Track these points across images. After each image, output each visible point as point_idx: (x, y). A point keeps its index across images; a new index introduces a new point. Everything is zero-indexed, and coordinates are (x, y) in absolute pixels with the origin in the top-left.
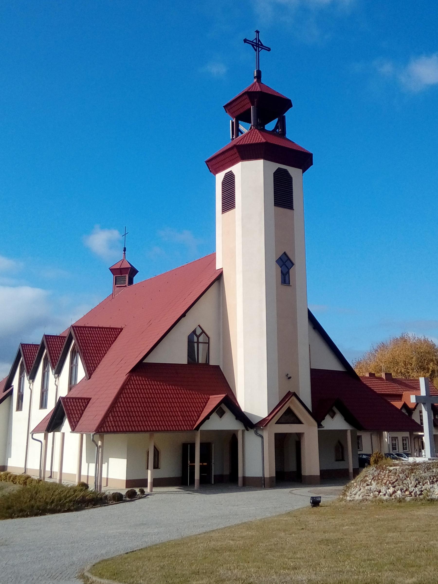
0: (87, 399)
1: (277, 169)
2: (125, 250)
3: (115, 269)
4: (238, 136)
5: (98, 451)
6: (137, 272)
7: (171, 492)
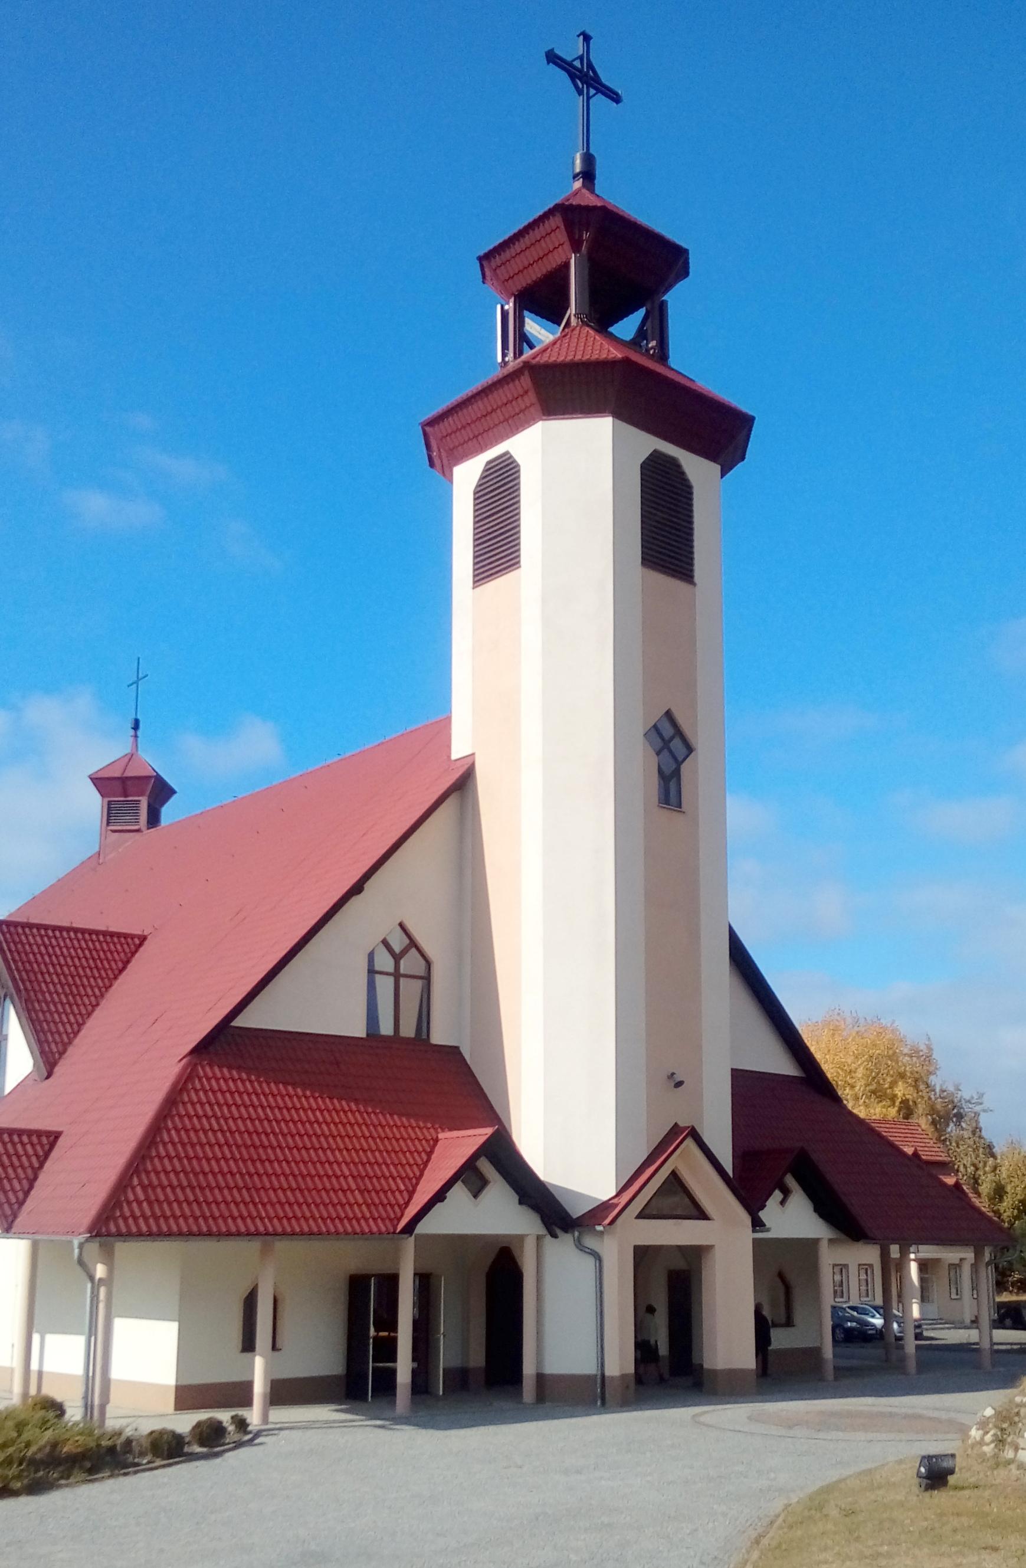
0: (48, 1134)
1: (651, 455)
2: (136, 726)
3: (109, 779)
4: (521, 353)
5: (95, 1297)
6: (172, 792)
7: (328, 1425)
